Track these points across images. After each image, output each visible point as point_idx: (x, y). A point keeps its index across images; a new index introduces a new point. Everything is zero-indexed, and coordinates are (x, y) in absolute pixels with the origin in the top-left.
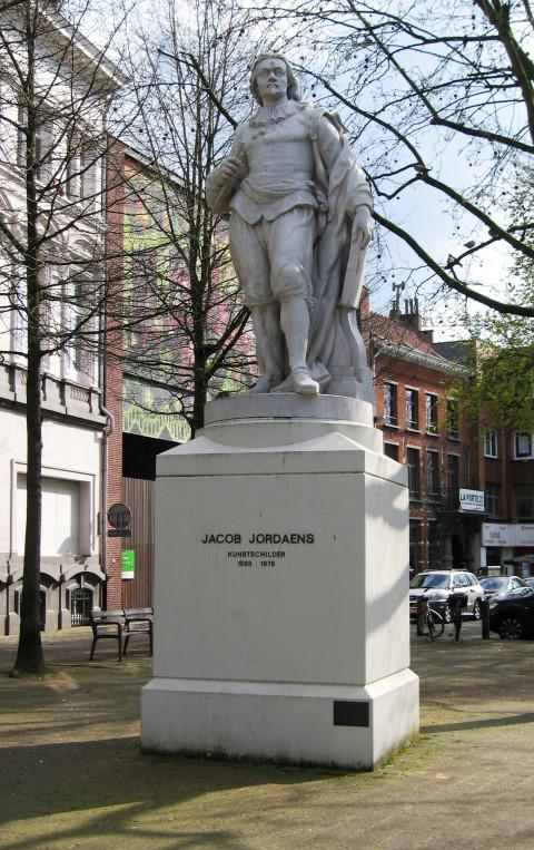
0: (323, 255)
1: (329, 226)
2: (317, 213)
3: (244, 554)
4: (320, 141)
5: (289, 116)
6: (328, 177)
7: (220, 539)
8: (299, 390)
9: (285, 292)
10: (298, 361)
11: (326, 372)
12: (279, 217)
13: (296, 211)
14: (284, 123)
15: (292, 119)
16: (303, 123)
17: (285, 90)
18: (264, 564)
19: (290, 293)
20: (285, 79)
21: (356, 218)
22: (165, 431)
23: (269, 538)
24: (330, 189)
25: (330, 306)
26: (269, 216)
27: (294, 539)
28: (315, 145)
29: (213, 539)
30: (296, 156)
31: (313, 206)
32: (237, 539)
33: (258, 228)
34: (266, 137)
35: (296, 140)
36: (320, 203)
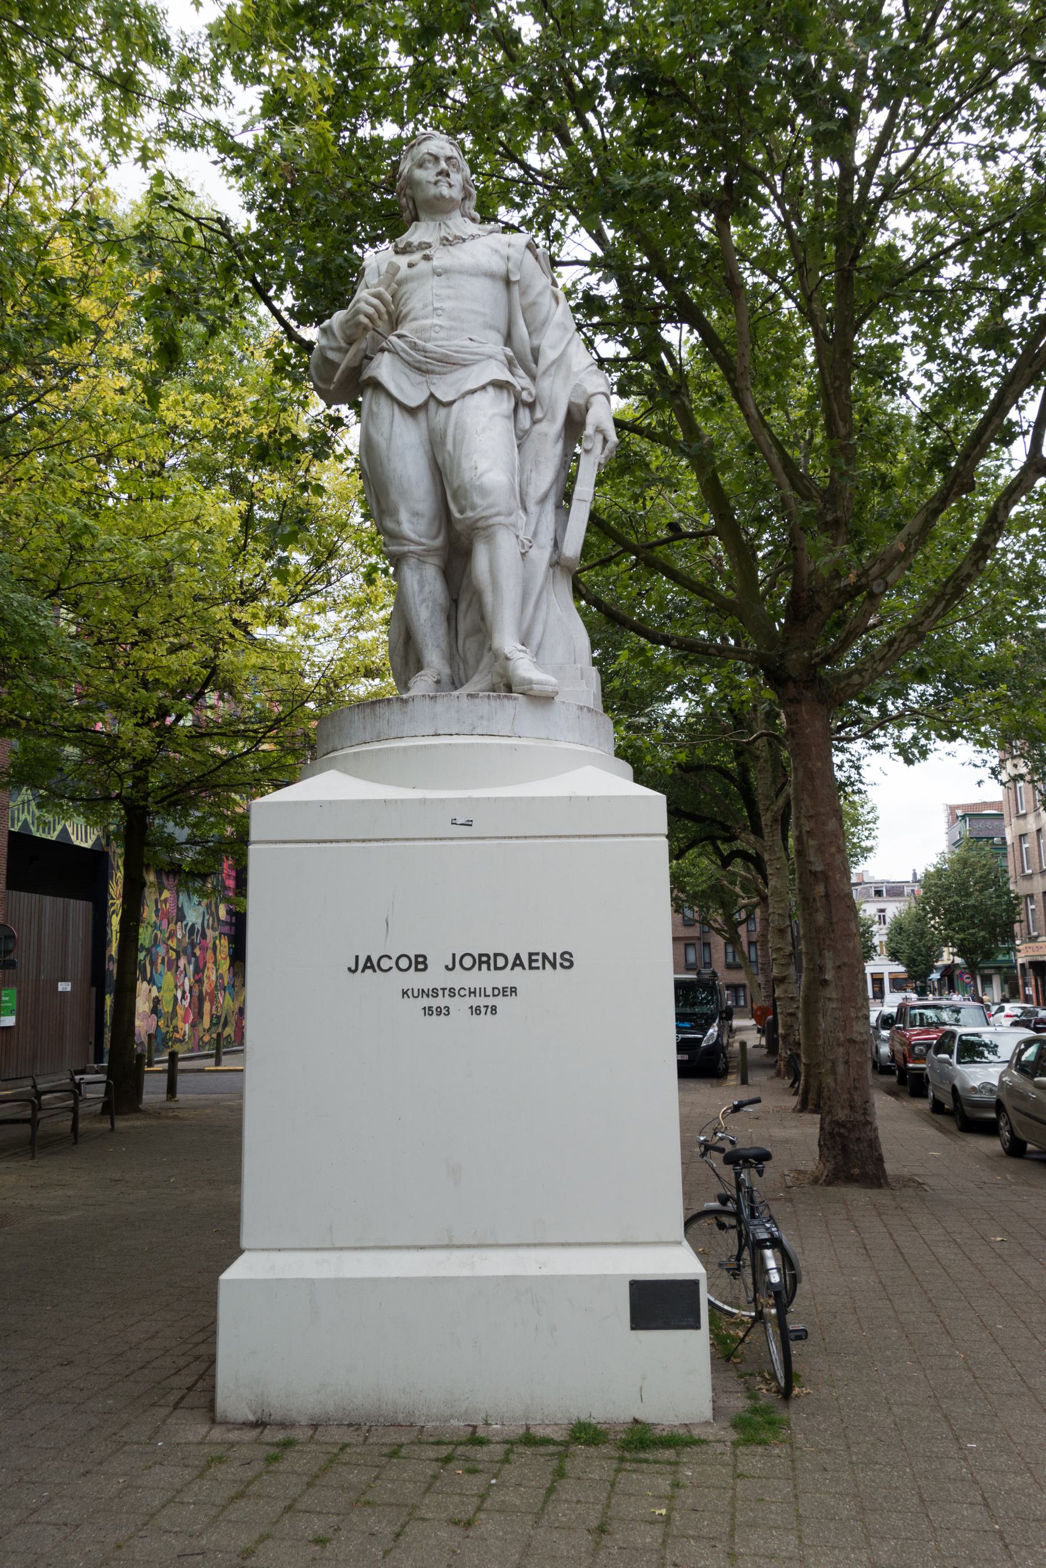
1: (538, 428)
7: (385, 964)
12: (463, 396)
13: (490, 390)
18: (476, 1011)
22: (64, 830)
23: (483, 961)
28: (516, 290)
29: (369, 964)
32: (420, 963)
35: (491, 276)
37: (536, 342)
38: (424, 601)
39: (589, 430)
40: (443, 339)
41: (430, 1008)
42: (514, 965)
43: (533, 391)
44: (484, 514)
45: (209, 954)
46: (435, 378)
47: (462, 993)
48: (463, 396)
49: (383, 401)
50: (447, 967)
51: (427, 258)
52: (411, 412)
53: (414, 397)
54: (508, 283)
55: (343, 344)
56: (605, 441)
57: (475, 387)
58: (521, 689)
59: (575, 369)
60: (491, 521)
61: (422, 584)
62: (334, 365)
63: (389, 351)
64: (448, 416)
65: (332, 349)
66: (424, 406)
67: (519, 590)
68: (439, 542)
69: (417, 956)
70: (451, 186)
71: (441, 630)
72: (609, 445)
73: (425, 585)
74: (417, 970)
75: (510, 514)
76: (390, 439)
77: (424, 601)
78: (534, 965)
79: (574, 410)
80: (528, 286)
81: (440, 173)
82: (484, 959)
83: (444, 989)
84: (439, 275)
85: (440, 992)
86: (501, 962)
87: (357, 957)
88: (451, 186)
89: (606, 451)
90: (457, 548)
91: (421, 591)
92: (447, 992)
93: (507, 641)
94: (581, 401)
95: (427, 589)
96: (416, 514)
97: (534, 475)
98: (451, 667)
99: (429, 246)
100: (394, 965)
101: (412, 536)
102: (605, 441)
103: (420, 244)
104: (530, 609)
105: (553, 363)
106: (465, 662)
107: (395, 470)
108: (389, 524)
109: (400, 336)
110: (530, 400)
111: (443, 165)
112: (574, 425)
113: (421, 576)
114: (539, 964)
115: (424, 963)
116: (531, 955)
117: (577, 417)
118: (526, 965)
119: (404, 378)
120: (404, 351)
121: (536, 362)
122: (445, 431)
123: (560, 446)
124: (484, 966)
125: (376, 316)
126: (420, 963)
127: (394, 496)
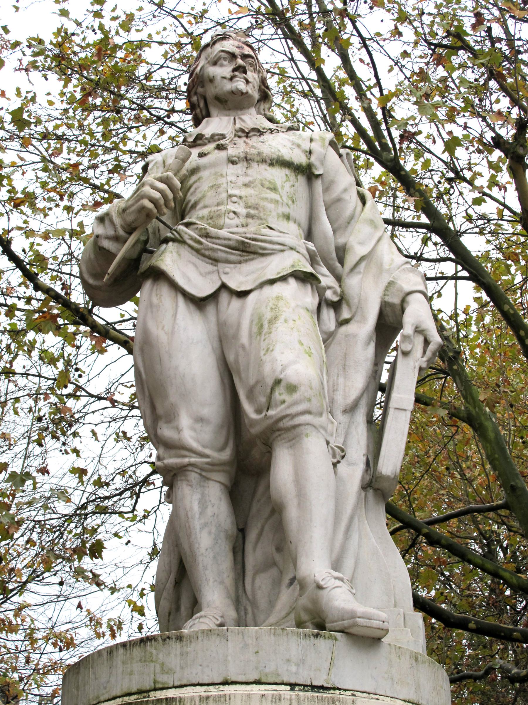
12: (261, 286)
37: (341, 241)
38: (205, 525)
39: (408, 329)
44: (289, 412)
46: (228, 268)
48: (261, 286)
49: (165, 290)
51: (220, 147)
52: (199, 303)
53: (201, 285)
55: (121, 232)
56: (427, 343)
58: (338, 625)
61: (203, 504)
62: (109, 256)
63: (174, 240)
64: (242, 310)
65: (108, 238)
66: (214, 297)
67: (331, 505)
68: (226, 455)
70: (247, 82)
71: (226, 563)
72: (432, 347)
73: (209, 506)
75: (321, 414)
76: (173, 332)
77: (205, 525)
79: (388, 310)
80: (332, 182)
88: (247, 82)
89: (429, 353)
90: (247, 462)
91: (202, 513)
93: (315, 564)
94: (396, 300)
95: (210, 511)
96: (200, 420)
97: (341, 380)
98: (237, 610)
99: (223, 136)
101: (195, 445)
103: (213, 136)
104: (340, 536)
106: (254, 604)
107: (176, 368)
108: (166, 432)
109: (188, 225)
110: (336, 299)
112: (387, 327)
113: (203, 495)
117: (391, 319)
119: (190, 266)
120: (192, 239)
121: (341, 261)
122: (239, 325)
123: (371, 349)
125: (162, 202)
127: (173, 397)
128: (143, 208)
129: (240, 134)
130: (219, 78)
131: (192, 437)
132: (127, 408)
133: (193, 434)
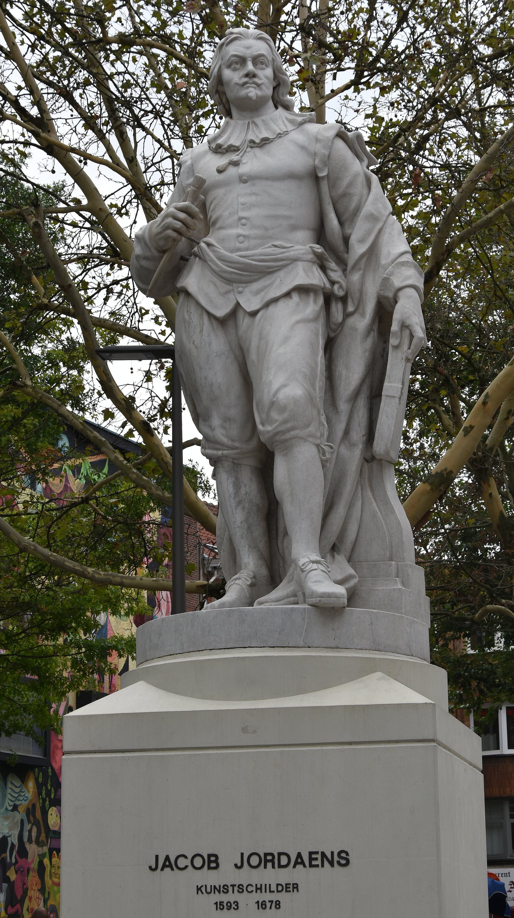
0: (341, 370)
1: (351, 321)
2: (329, 299)
3: (225, 889)
4: (333, 180)
5: (279, 136)
6: (346, 240)
7: (182, 862)
8: (313, 600)
9: (284, 432)
10: (304, 551)
11: (352, 571)
12: (267, 305)
13: (295, 297)
14: (272, 147)
15: (285, 140)
16: (303, 148)
17: (269, 92)
18: (262, 905)
19: (288, 436)
20: (269, 72)
21: (398, 307)
23: (268, 860)
24: (351, 262)
25: (354, 456)
26: (250, 302)
27: (316, 859)
28: (325, 186)
30: (296, 201)
31: (323, 288)
32: (212, 862)
33: (230, 324)
34: (244, 169)
35: (291, 176)
36: (333, 283)
40: (247, 249)
41: (221, 903)
42: (296, 863)
43: (344, 284)
44: (280, 429)
45: (33, 879)
47: (250, 889)
48: (267, 305)
49: (193, 308)
50: (236, 865)
54: (316, 179)
55: (155, 253)
57: (279, 293)
59: (383, 262)
60: (288, 436)
69: (209, 856)
74: (209, 868)
78: (314, 863)
81: (247, 75)
82: (269, 858)
83: (233, 886)
84: (245, 182)
85: (230, 889)
86: (284, 860)
87: (157, 857)
92: (236, 888)
95: (243, 491)
100: (189, 864)
101: (225, 440)
102: (412, 336)
105: (362, 256)
111: (250, 66)
114: (319, 862)
115: (216, 861)
116: (311, 853)
118: (307, 863)
124: (269, 865)
125: (184, 229)
126: (212, 862)
128: (168, 238)
129: (252, 144)
130: (232, 83)
131: (222, 435)
132: (369, 32)
133: (223, 432)
